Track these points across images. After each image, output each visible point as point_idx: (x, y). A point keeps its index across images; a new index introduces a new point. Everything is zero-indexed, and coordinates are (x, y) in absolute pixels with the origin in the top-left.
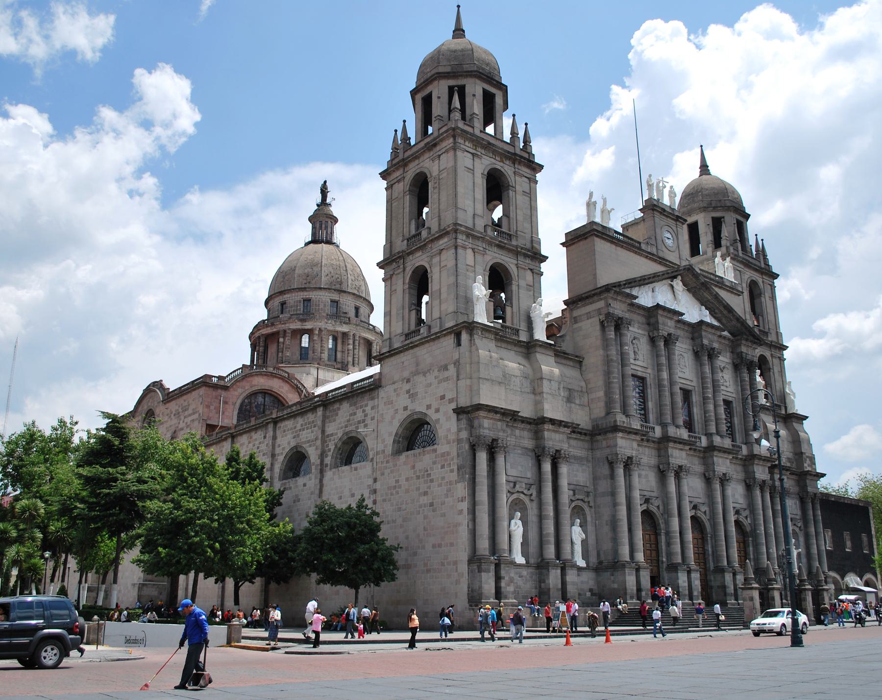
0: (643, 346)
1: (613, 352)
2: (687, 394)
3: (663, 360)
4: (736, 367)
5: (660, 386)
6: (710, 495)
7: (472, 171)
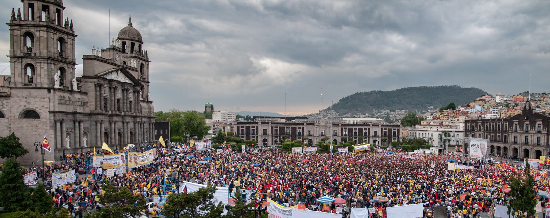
0: (107, 90)
1: (98, 93)
2: (119, 101)
3: (113, 94)
4: (134, 92)
5: (111, 100)
6: (123, 126)
7: (53, 39)
